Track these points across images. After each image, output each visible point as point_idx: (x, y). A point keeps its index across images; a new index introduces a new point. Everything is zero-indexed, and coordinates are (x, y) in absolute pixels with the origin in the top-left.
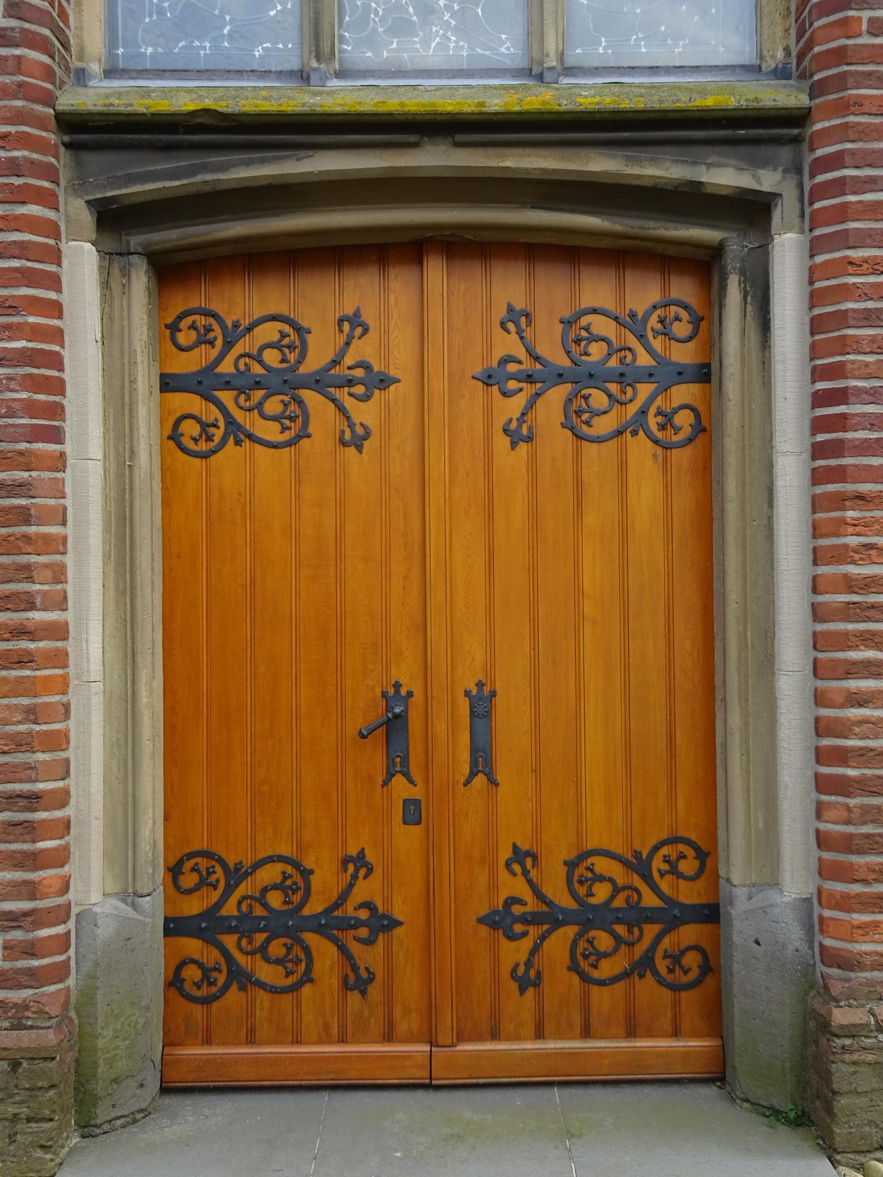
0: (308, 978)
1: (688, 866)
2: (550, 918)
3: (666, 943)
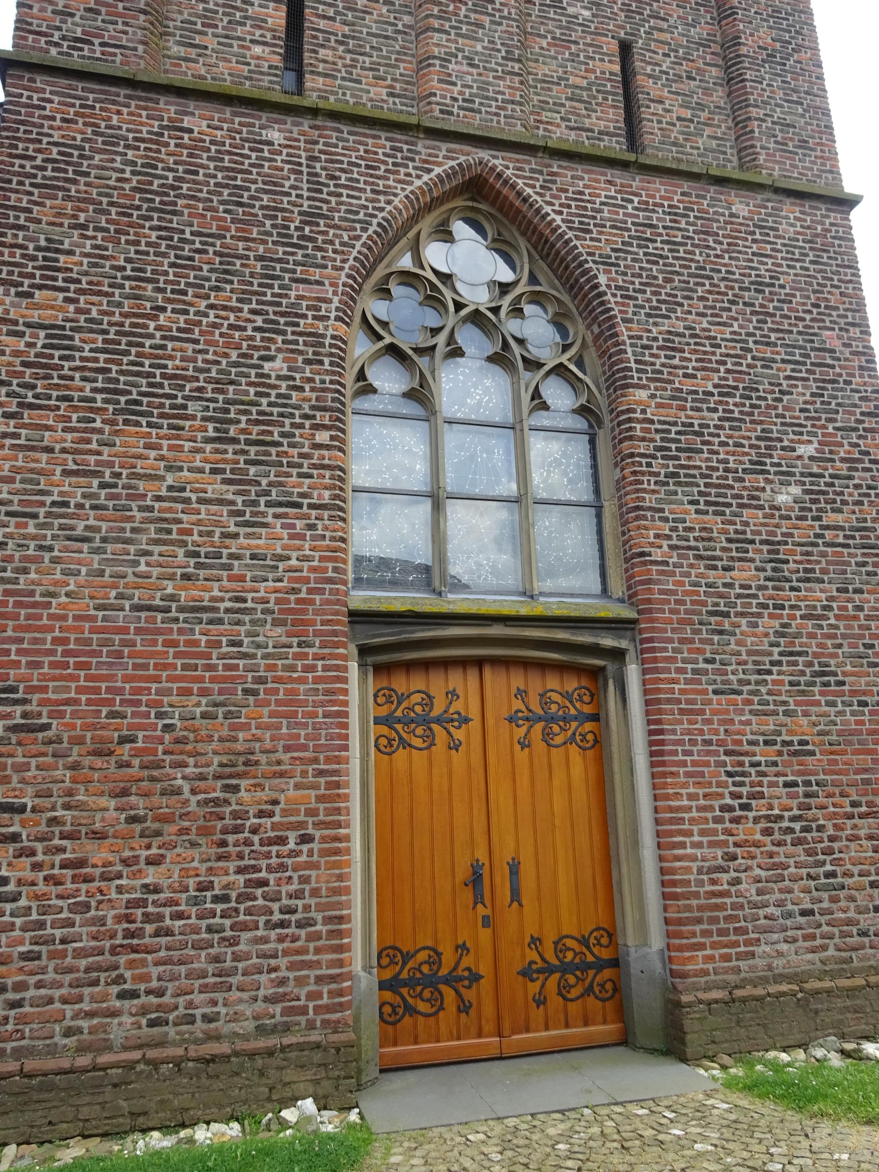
0: (441, 1008)
1: (605, 941)
2: (549, 970)
3: (598, 979)
